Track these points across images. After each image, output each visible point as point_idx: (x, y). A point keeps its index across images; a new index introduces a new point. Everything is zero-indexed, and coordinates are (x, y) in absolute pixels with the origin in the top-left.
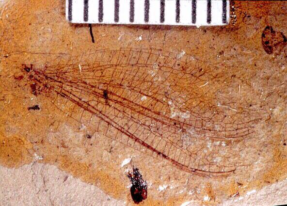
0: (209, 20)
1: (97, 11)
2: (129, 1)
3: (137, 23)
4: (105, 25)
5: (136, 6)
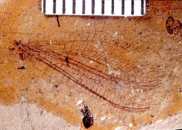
0: (133, 13)
1: (62, 7)
2: (82, 0)
3: (87, 15)
4: (67, 16)
5: (86, 4)
